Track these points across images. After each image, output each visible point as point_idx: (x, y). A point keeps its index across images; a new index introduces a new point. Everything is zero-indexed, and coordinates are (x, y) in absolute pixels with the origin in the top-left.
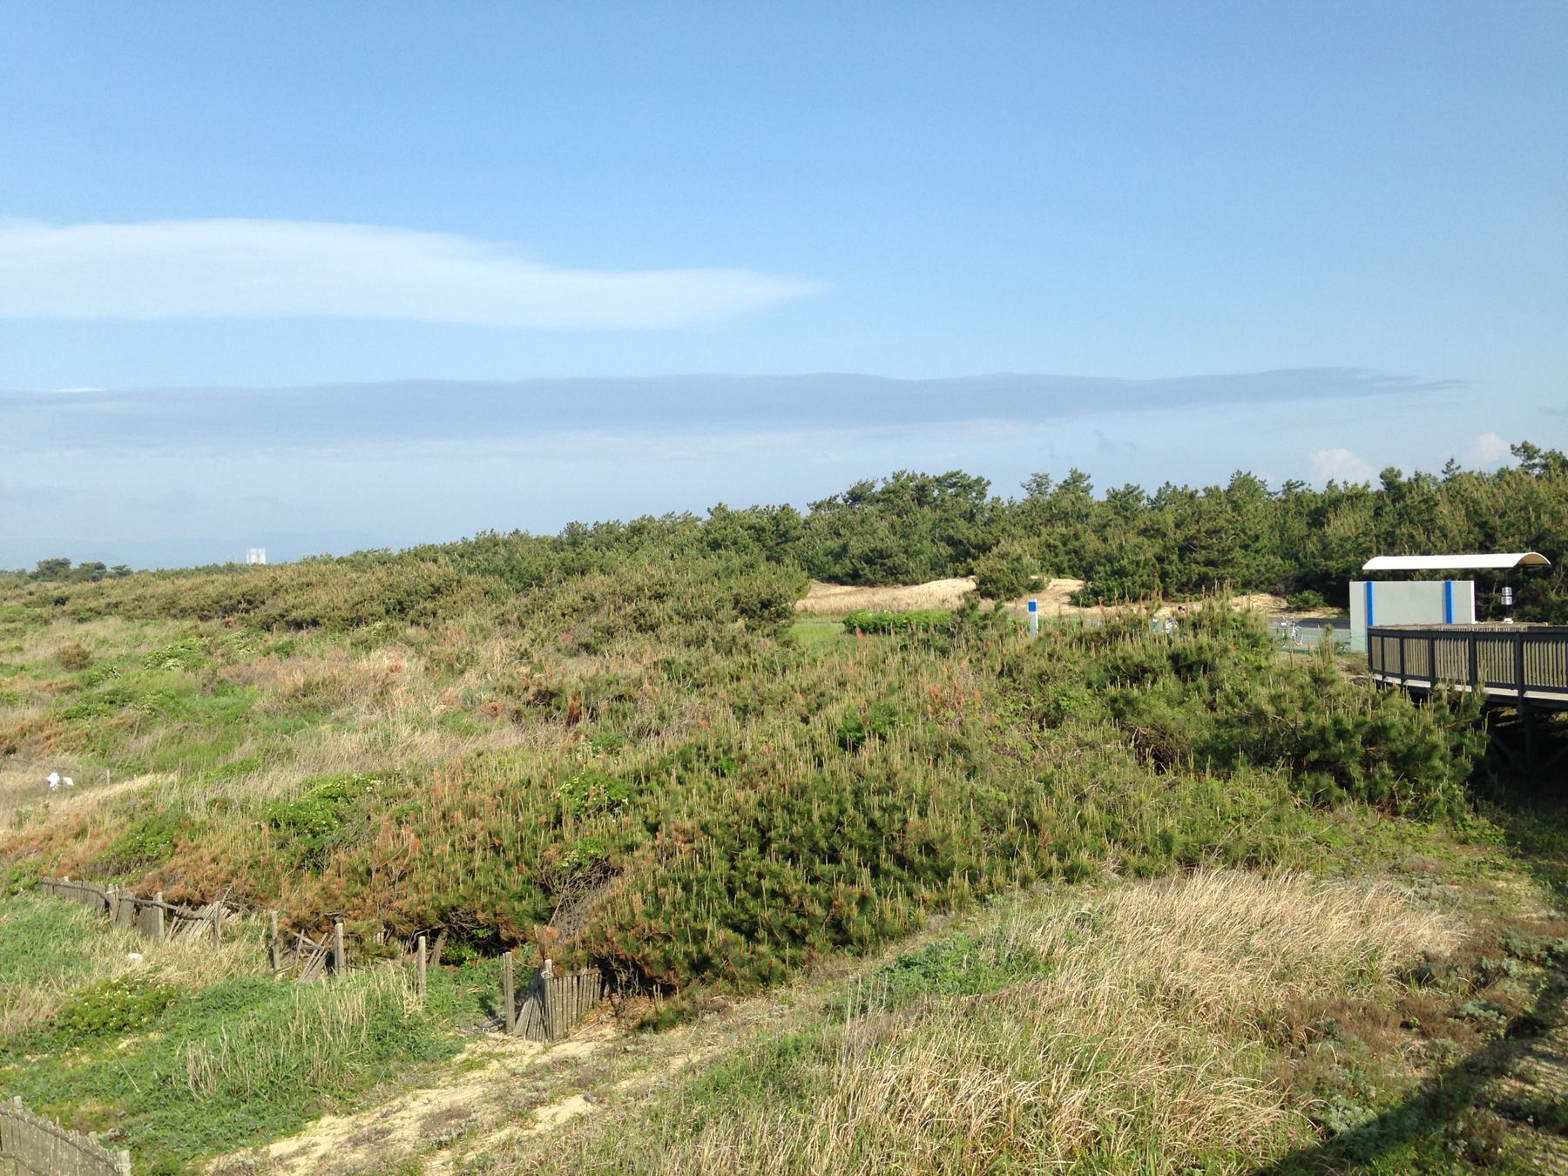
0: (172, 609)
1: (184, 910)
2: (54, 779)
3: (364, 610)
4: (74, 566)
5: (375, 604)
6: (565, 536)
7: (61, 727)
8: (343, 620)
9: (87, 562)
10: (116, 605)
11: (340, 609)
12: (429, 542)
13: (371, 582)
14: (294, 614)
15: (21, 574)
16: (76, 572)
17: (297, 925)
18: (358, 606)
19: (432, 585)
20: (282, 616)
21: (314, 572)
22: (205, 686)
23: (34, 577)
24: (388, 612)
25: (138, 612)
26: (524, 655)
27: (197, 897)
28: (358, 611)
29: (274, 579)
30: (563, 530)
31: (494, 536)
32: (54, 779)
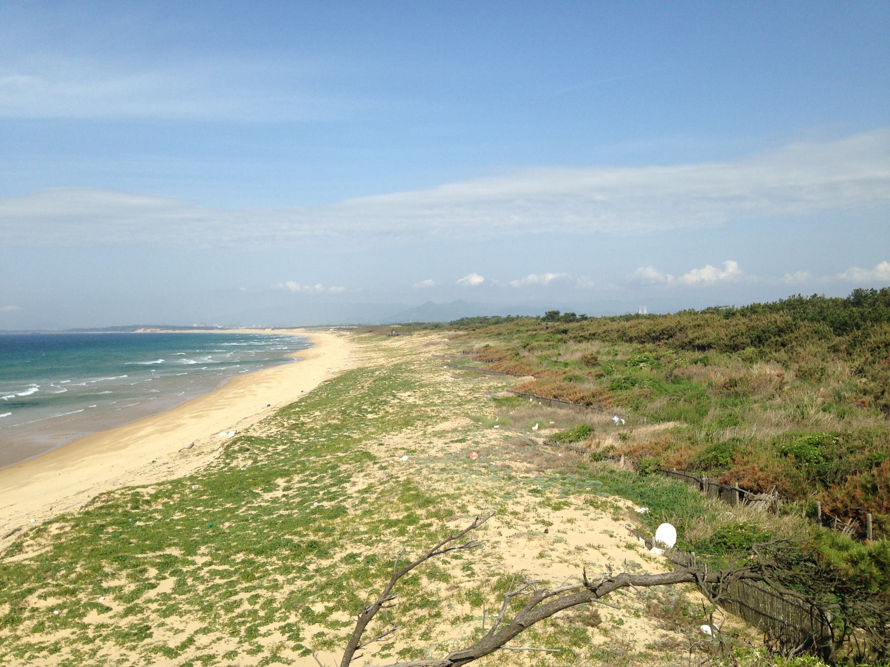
0: (624, 337)
1: (747, 493)
2: (616, 419)
3: (740, 340)
4: (562, 314)
5: (744, 337)
6: (852, 297)
7: (611, 394)
8: (726, 346)
9: (568, 312)
10: (594, 335)
11: (723, 340)
12: (757, 302)
13: (742, 323)
14: (697, 342)
15: (538, 318)
16: (563, 317)
17: (834, 511)
18: (734, 339)
19: (778, 327)
20: (690, 343)
21: (29, 407)
22: (667, 378)
23: (544, 320)
24: (752, 341)
25: (608, 338)
26: (860, 372)
27: (756, 488)
28: (734, 341)
29: (679, 322)
30: (851, 294)
31: (801, 298)
32: (616, 419)
